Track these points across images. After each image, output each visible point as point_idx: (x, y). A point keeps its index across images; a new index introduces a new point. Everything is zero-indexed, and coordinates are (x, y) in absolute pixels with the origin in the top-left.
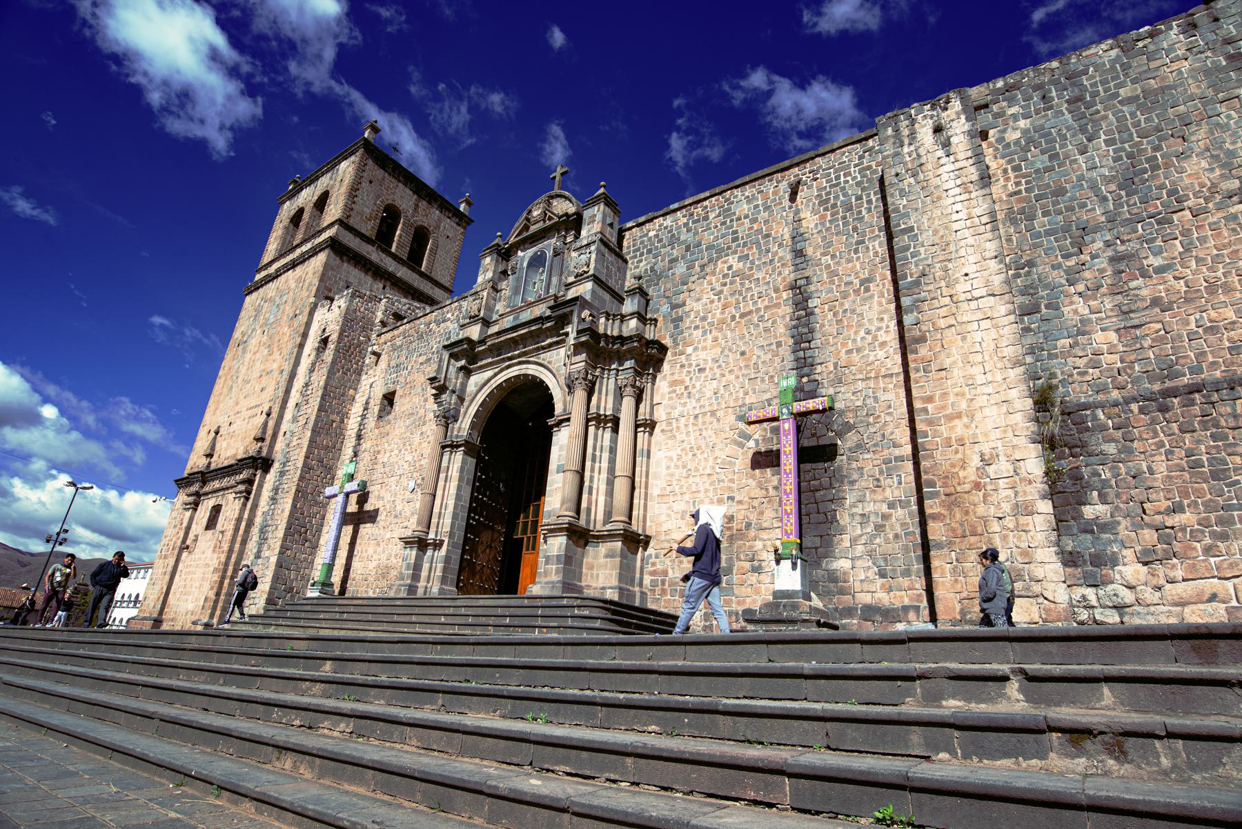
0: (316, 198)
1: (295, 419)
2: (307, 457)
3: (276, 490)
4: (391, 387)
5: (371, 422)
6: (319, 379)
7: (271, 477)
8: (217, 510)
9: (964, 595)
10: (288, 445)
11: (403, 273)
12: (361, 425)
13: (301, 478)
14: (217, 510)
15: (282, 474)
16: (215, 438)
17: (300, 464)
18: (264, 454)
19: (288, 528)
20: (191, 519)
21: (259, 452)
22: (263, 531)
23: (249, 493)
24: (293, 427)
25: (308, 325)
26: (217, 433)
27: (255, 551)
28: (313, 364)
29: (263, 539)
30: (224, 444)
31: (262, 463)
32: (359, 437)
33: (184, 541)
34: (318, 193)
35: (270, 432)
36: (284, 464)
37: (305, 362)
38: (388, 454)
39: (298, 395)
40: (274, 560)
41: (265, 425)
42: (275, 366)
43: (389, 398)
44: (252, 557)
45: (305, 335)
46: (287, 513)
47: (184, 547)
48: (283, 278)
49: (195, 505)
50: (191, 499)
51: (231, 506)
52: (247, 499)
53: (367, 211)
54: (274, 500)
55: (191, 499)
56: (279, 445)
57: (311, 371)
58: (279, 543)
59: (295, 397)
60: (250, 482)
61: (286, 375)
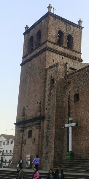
0: (36, 33)
1: (49, 104)
2: (56, 115)
3: (48, 126)
4: (77, 93)
5: (72, 103)
6: (54, 92)
7: (45, 121)
8: (30, 132)
9: (35, 139)
10: (49, 112)
11: (67, 51)
12: (69, 105)
13: (56, 122)
14: (30, 132)
15: (49, 121)
16: (24, 111)
17: (54, 118)
18: (42, 115)
19: (55, 137)
20: (23, 134)
21: (40, 115)
22: (47, 138)
23: (40, 127)
24: (49, 107)
25: (46, 75)
26: (24, 109)
27: (46, 144)
28: (51, 87)
29: (48, 140)
30: (27, 113)
31: (42, 118)
32: (69, 108)
33: (22, 141)
34: (37, 31)
35: (42, 109)
36: (49, 118)
37: (48, 88)
38: (81, 113)
39: (48, 97)
40: (53, 146)
41: (40, 106)
42: (38, 88)
43: (77, 96)
44: (45, 146)
45: (46, 79)
46: (54, 132)
47: (23, 143)
48: (32, 60)
49: (23, 131)
50: (22, 129)
51: (36, 132)
52: (40, 129)
53: (54, 35)
54: (48, 128)
55: (22, 129)
56: (46, 112)
57: (50, 90)
58: (54, 141)
59: (47, 98)
60: (39, 124)
61: (42, 91)
